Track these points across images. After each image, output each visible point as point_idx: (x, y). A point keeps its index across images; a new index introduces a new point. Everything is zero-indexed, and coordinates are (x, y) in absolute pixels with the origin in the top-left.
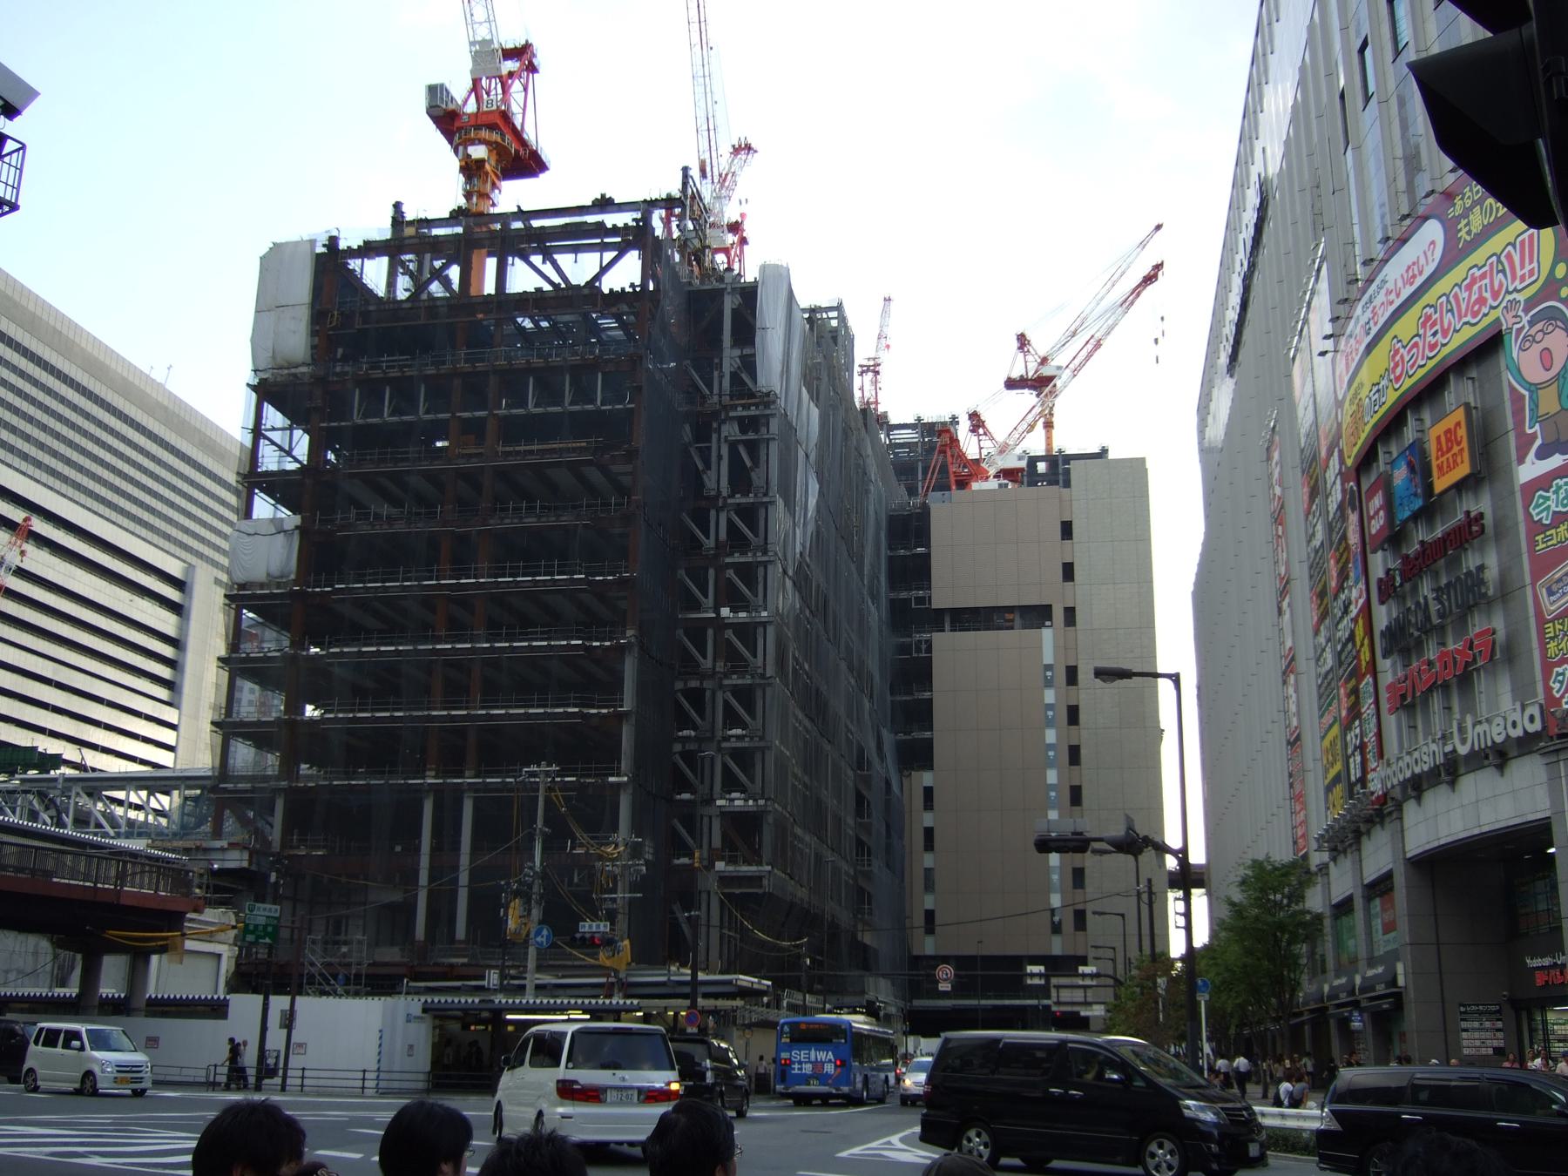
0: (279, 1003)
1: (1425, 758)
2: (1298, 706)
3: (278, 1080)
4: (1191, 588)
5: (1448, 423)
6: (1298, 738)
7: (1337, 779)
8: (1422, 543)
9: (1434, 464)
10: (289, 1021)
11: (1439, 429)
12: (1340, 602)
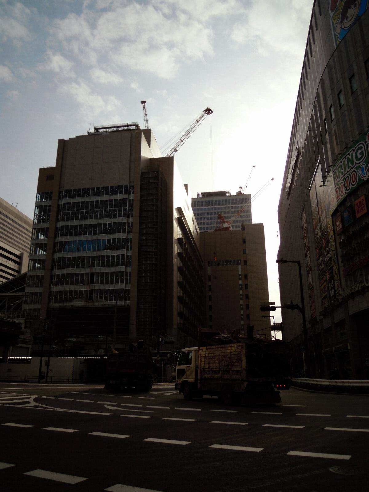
0: (45, 359)
1: (356, 288)
2: (312, 279)
3: (45, 380)
4: (277, 254)
5: (360, 199)
6: (313, 287)
7: (326, 296)
8: (353, 231)
9: (356, 210)
10: (48, 363)
11: (357, 201)
12: (326, 250)
